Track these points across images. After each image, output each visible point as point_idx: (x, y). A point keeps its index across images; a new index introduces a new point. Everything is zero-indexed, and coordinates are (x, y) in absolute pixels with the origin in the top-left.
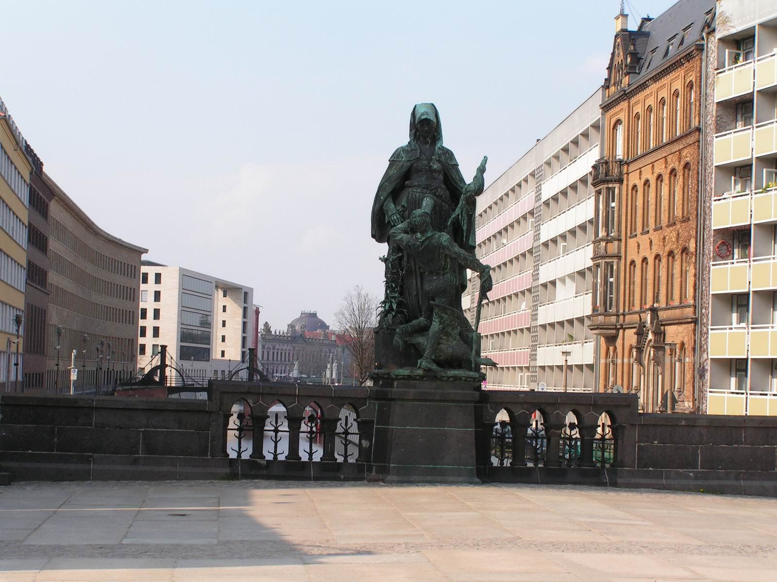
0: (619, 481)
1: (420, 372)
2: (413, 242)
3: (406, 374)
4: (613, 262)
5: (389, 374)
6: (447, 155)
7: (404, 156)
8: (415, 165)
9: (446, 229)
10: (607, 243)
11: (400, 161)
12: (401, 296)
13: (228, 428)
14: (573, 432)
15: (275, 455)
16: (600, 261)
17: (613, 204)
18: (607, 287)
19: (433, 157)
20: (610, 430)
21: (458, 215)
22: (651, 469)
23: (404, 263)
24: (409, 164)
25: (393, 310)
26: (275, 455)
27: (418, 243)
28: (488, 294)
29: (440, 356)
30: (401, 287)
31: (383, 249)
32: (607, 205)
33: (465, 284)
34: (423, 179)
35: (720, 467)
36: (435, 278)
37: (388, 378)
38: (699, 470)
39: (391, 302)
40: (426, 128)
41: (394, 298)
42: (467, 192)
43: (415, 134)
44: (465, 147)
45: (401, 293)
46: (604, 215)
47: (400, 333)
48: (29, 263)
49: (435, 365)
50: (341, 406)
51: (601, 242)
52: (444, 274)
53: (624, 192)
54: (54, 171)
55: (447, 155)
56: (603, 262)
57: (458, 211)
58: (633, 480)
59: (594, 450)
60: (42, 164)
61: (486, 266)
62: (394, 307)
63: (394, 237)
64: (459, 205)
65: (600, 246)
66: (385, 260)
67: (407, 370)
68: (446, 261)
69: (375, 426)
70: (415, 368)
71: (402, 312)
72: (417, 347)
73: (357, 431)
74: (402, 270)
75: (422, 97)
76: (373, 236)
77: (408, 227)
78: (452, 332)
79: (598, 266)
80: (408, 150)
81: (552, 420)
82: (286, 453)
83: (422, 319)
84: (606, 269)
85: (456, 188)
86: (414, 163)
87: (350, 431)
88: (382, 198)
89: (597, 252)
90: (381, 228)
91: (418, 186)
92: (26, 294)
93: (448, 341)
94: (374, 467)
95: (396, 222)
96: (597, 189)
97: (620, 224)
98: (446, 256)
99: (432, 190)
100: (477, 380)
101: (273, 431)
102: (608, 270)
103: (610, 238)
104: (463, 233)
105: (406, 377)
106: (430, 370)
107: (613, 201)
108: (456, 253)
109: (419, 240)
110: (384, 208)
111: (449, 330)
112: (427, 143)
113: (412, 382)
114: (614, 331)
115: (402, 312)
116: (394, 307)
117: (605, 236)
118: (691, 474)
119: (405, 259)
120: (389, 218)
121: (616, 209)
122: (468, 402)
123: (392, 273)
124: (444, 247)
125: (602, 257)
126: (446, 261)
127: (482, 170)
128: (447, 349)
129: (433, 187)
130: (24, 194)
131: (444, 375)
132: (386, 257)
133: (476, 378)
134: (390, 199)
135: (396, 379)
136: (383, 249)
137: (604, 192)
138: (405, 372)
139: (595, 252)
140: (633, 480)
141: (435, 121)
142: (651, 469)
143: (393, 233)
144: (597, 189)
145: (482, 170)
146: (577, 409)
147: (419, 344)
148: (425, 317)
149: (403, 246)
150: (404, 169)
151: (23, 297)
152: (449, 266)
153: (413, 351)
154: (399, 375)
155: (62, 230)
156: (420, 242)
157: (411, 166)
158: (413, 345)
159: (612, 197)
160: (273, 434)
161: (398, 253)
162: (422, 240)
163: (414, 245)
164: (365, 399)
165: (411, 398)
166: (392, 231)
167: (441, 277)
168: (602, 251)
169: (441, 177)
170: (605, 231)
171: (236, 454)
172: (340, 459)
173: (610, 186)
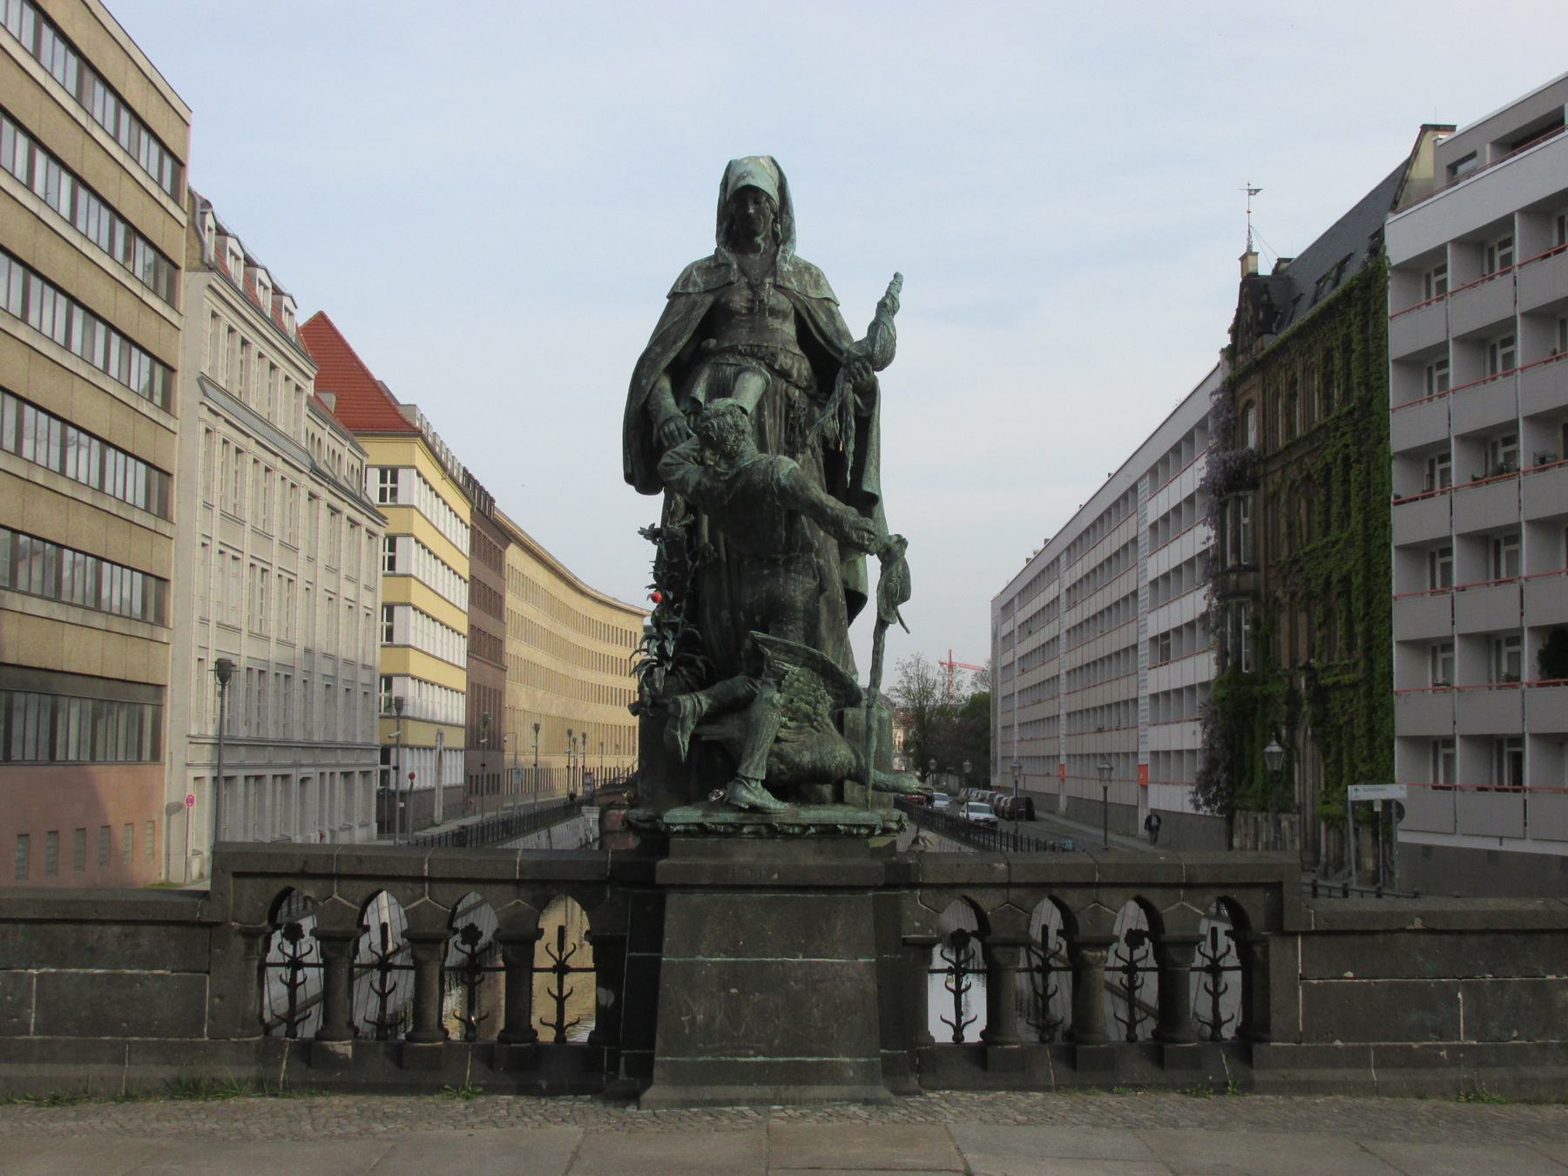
0: (1257, 1076)
14: (1138, 953)
15: (560, 1027)
20: (1233, 944)
22: (1338, 1043)
24: (709, 299)
25: (668, 659)
26: (958, 1029)
28: (902, 608)
31: (652, 508)
35: (1515, 1034)
38: (1463, 1041)
40: (751, 215)
41: (674, 627)
44: (840, 253)
48: (472, 627)
50: (543, 904)
54: (508, 507)
58: (1302, 1075)
60: (492, 500)
62: (670, 649)
66: (652, 534)
71: (690, 663)
73: (591, 964)
75: (749, 142)
76: (629, 478)
81: (1085, 929)
82: (1238, 1021)
87: (571, 962)
90: (644, 465)
92: (468, 670)
101: (1124, 969)
104: (849, 468)
115: (690, 663)
116: (670, 649)
118: (1443, 1053)
123: (671, 566)
127: (887, 307)
130: (463, 538)
132: (658, 526)
136: (652, 508)
140: (1302, 1075)
142: (1338, 1043)
145: (887, 307)
151: (464, 675)
155: (529, 587)
160: (553, 978)
165: (707, 882)
169: (789, 329)
171: (951, 1032)
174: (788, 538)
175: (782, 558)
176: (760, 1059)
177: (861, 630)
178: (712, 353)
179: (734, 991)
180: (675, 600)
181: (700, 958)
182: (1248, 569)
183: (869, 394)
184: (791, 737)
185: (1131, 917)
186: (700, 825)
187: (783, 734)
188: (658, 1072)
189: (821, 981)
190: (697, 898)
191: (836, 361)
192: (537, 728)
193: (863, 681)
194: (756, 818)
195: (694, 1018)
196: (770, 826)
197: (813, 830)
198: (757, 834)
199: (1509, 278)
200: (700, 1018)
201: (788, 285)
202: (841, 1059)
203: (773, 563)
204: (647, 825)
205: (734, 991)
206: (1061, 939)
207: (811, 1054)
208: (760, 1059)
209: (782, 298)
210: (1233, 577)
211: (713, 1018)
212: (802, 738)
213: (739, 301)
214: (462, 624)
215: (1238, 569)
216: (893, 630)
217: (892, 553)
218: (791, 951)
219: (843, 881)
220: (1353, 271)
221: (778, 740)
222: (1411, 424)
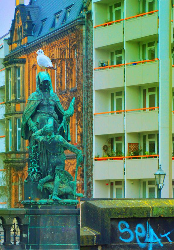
1: (51, 201)
3: (45, 202)
4: (20, 117)
5: (36, 202)
8: (42, 102)
9: (57, 133)
10: (15, 104)
11: (34, 100)
13: (11, 230)
16: (11, 116)
17: (19, 78)
18: (16, 135)
21: (63, 126)
23: (39, 150)
24: (39, 102)
27: (48, 140)
29: (60, 193)
30: (38, 161)
32: (15, 79)
34: (46, 110)
37: (35, 204)
39: (34, 168)
42: (66, 115)
45: (38, 164)
46: (13, 85)
47: (41, 183)
49: (58, 197)
51: (12, 104)
52: (60, 155)
53: (27, 70)
56: (14, 118)
57: (62, 124)
63: (35, 137)
64: (63, 121)
65: (10, 106)
68: (61, 149)
69: (29, 227)
70: (48, 199)
71: (40, 173)
72: (48, 189)
74: (38, 153)
77: (42, 133)
78: (64, 182)
79: (9, 120)
80: (37, 95)
83: (49, 176)
84: (15, 122)
85: (60, 112)
86: (41, 101)
88: (27, 118)
89: (8, 110)
91: (44, 113)
94: (30, 246)
95: (35, 130)
96: (7, 67)
97: (24, 92)
98: (61, 146)
99: (50, 114)
102: (17, 123)
103: (17, 101)
105: (45, 203)
106: (56, 200)
107: (19, 76)
108: (66, 145)
109: (49, 139)
110: (28, 123)
111: (64, 181)
112: (46, 91)
114: (22, 164)
115: (40, 173)
117: (14, 99)
119: (39, 147)
120: (31, 128)
121: (21, 81)
122: (73, 214)
124: (61, 142)
125: (13, 114)
126: (61, 149)
128: (63, 190)
129: (51, 113)
131: (62, 202)
134: (30, 119)
135: (40, 205)
137: (12, 70)
138: (44, 201)
139: (7, 110)
143: (35, 135)
144: (7, 67)
146: (3, 217)
147: (49, 188)
148: (50, 175)
150: (37, 105)
154: (42, 203)
157: (40, 103)
158: (46, 188)
159: (18, 73)
161: (36, 145)
163: (46, 141)
164: (24, 214)
166: (34, 134)
167: (59, 156)
168: (13, 110)
169: (53, 108)
170: (14, 96)
172: (13, 243)
173: (17, 65)
174: (60, 150)
175: (59, 154)
176: (58, 245)
178: (39, 113)
179: (53, 233)
181: (47, 227)
182: (21, 101)
185: (15, 221)
187: (60, 186)
188: (40, 247)
189: (68, 231)
190: (46, 216)
191: (62, 115)
194: (56, 202)
195: (46, 238)
196: (58, 203)
197: (66, 204)
199: (120, 25)
200: (47, 237)
202: (71, 244)
203: (57, 155)
204: (34, 203)
205: (53, 233)
206: (17, 226)
207: (66, 244)
208: (58, 245)
210: (13, 105)
211: (49, 237)
215: (15, 102)
218: (62, 225)
219: (71, 213)
220: (72, 16)
222: (103, 79)
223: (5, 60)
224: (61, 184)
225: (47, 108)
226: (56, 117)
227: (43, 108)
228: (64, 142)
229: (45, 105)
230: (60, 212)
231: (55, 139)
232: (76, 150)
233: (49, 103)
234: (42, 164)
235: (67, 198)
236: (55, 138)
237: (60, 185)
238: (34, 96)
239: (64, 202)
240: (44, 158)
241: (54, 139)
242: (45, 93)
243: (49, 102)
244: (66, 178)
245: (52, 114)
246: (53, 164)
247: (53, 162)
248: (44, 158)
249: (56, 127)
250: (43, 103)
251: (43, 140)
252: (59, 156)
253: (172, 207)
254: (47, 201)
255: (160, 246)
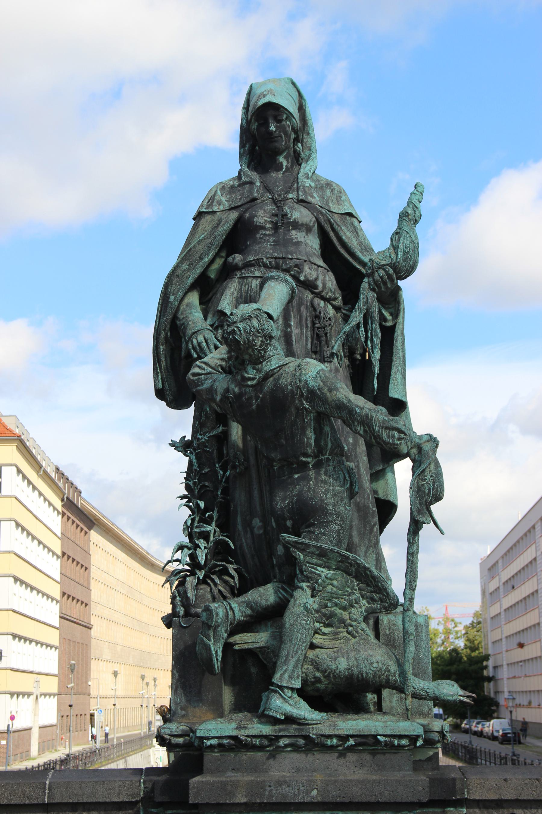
2: (236, 390)
6: (328, 192)
7: (223, 199)
8: (247, 215)
12: (221, 531)
19: (290, 196)
21: (358, 326)
24: (234, 215)
33: (391, 499)
36: (296, 476)
40: (270, 134)
43: (253, 147)
44: (354, 167)
49: (303, 704)
55: (328, 192)
59: (265, 210)
61: (426, 438)
67: (230, 722)
76: (160, 394)
86: (246, 210)
93: (334, 639)
100: (420, 743)
106: (290, 720)
113: (246, 756)
123: (203, 477)
127: (409, 217)
133: (418, 736)
141: (293, 109)
145: (409, 217)
149: (217, 405)
152: (330, 445)
153: (253, 670)
154: (208, 738)
156: (252, 386)
162: (255, 382)
169: (313, 242)
177: (392, 544)
180: (206, 509)
183: (391, 299)
184: (327, 643)
186: (235, 738)
187: (318, 640)
192: (142, 706)
193: (397, 586)
194: (292, 729)
196: (306, 737)
197: (351, 742)
198: (296, 748)
201: (310, 199)
209: (305, 211)
212: (337, 644)
213: (263, 217)
214: (55, 591)
216: (427, 530)
217: (423, 454)
221: (313, 646)
223: (301, 130)
224: (325, 630)
225: (272, 239)
226: (320, 284)
227: (255, 242)
228: (325, 390)
229: (263, 228)
230: (315, 792)
231: (283, 381)
232: (396, 434)
233: (285, 215)
234: (247, 525)
235: (357, 708)
236: (280, 376)
237: (317, 632)
238: (219, 193)
239: (341, 733)
240: (256, 493)
241: (276, 381)
242: (274, 175)
243: (286, 209)
244: (357, 594)
245: (297, 266)
246: (285, 520)
247: (282, 509)
248: (256, 493)
249: (321, 332)
250: (253, 216)
251: (227, 390)
252: (312, 473)
253: (382, 267)
254: (239, 728)
255: (314, 742)
